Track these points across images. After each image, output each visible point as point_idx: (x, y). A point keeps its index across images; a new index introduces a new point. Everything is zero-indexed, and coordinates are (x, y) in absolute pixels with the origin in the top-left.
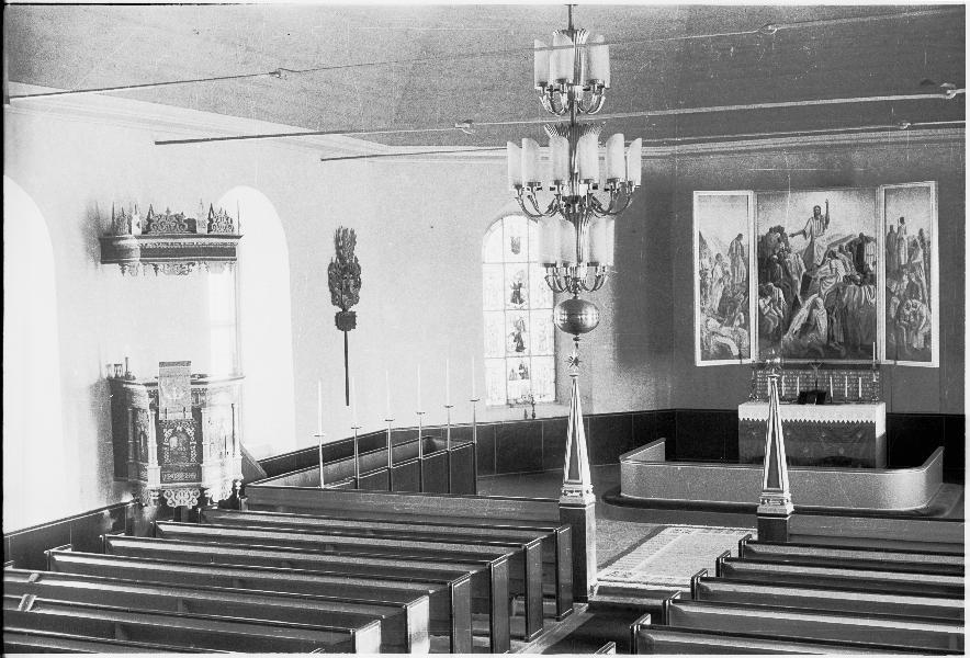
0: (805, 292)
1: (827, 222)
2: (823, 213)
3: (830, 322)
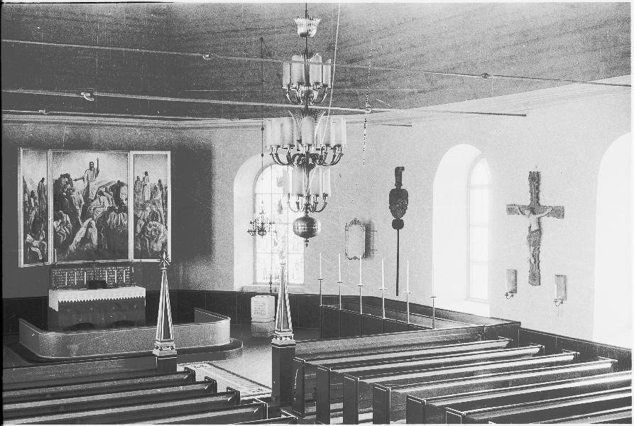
1: (98, 172)
2: (95, 166)
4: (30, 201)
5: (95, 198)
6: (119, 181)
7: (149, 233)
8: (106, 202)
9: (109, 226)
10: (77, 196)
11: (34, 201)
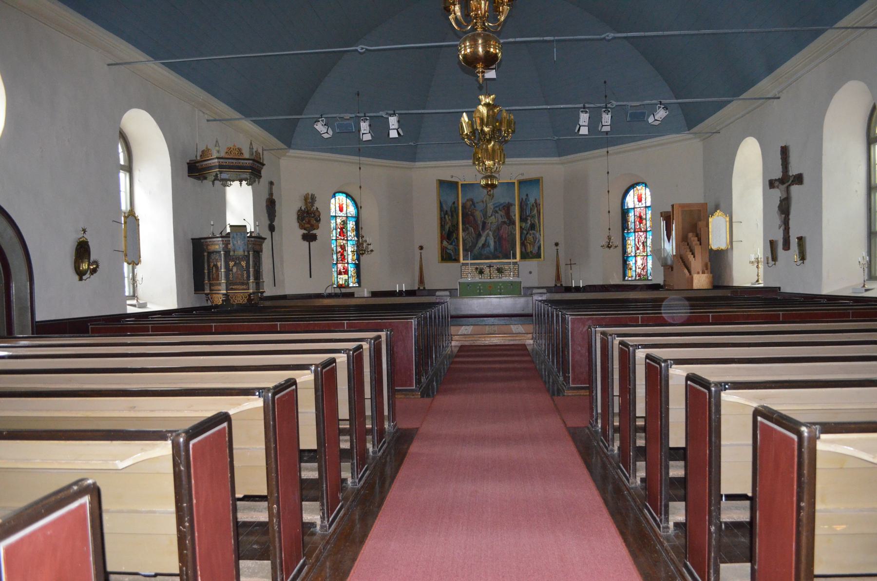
3: (495, 242)
8: (500, 217)
10: (479, 215)
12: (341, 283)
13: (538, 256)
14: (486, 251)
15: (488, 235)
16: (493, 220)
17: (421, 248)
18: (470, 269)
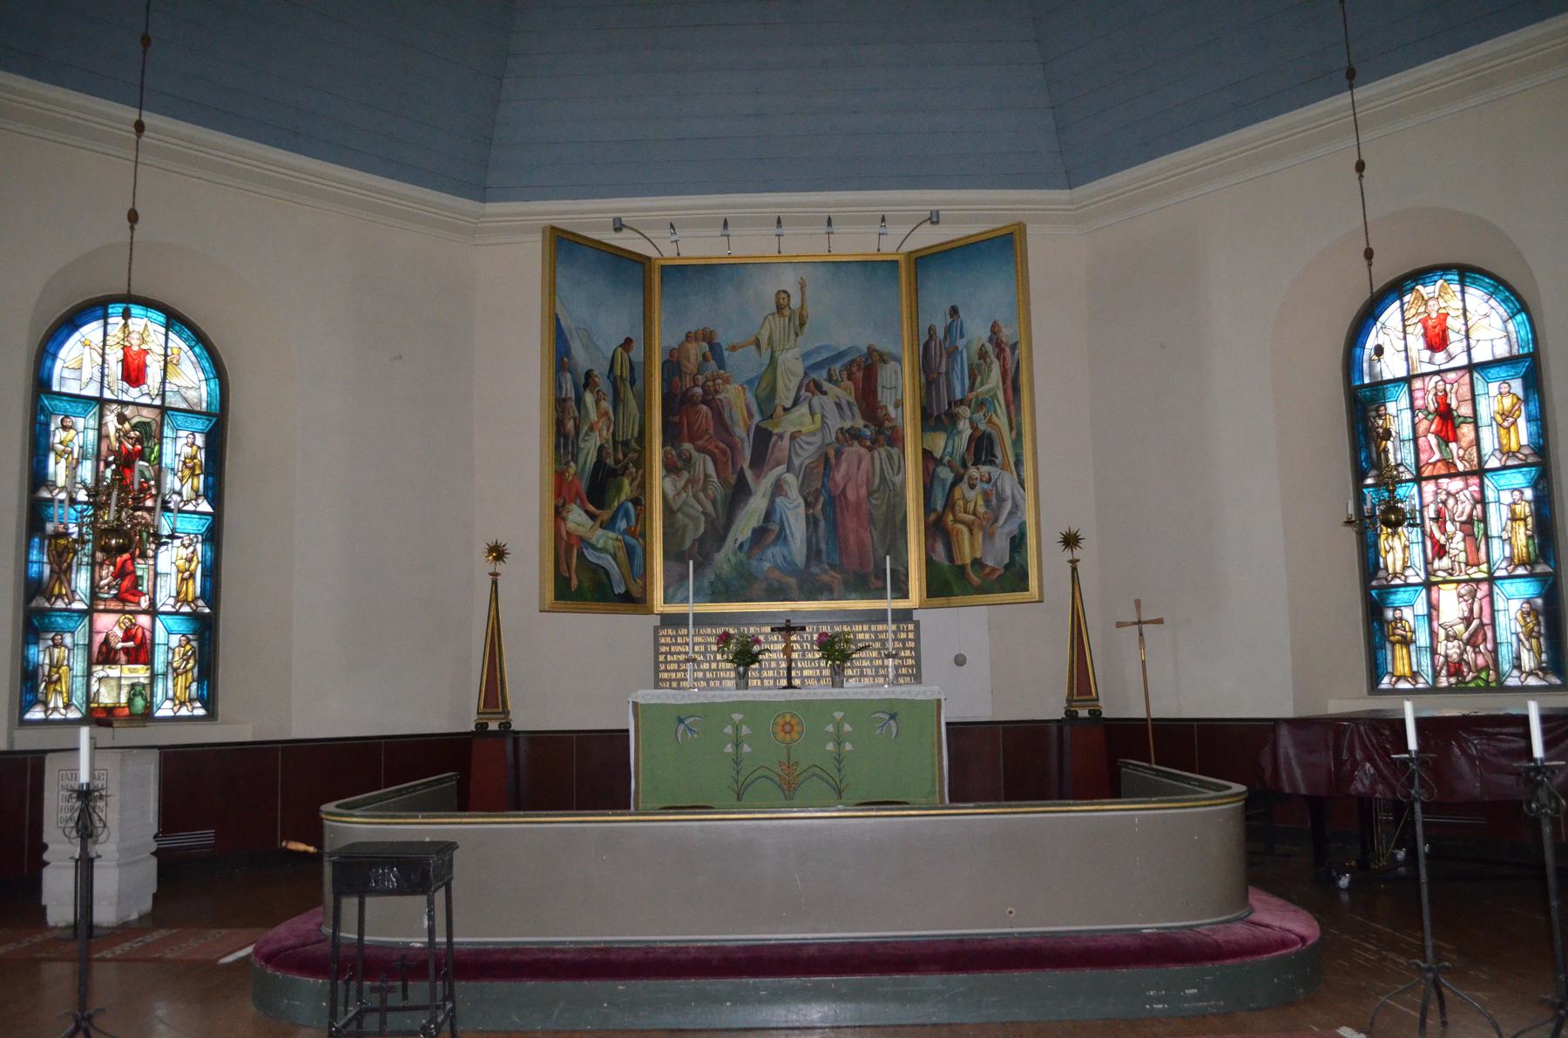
0: (760, 460)
1: (802, 324)
2: (795, 302)
3: (812, 522)
4: (579, 401)
5: (796, 402)
6: (871, 350)
7: (971, 507)
9: (844, 492)
10: (737, 398)
11: (597, 402)
12: (106, 698)
13: (1014, 577)
14: (768, 561)
15: (778, 489)
16: (808, 425)
17: (498, 552)
18: (697, 641)
